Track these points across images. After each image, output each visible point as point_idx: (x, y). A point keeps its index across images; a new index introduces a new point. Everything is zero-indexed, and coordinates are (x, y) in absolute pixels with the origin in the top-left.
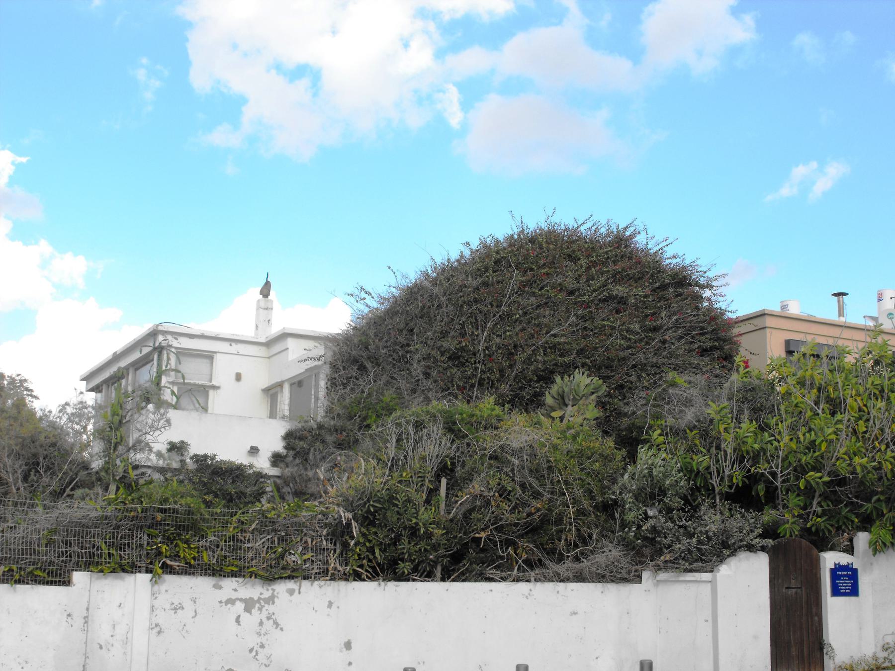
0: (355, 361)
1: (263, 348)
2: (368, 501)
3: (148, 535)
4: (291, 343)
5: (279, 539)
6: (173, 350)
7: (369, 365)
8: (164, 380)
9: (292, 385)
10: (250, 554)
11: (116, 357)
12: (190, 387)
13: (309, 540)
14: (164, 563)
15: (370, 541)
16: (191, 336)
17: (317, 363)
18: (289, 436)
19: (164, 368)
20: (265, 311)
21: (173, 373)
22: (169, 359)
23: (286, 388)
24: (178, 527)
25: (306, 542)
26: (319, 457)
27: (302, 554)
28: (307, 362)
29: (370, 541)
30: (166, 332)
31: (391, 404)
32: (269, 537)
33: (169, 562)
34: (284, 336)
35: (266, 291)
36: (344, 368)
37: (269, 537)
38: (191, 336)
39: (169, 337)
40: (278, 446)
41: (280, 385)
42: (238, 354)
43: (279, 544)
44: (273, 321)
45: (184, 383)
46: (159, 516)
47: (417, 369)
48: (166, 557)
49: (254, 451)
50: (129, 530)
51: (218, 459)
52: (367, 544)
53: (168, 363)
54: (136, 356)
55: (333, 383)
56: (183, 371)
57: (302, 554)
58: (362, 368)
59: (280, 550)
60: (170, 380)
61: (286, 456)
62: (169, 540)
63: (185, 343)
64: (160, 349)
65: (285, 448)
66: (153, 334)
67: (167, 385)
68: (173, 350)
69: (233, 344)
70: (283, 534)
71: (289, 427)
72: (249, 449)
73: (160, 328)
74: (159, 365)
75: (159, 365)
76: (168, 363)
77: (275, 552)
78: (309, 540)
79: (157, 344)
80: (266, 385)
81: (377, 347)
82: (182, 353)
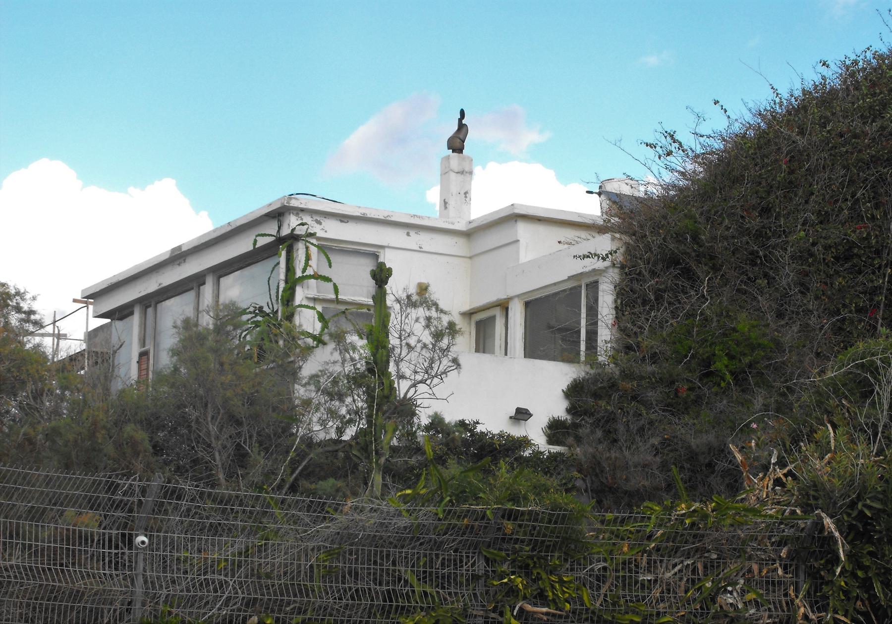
0: (673, 261)
1: (461, 241)
2: (859, 498)
3: (487, 560)
4: (523, 230)
5: (705, 567)
6: (314, 241)
7: (700, 270)
8: (300, 296)
9: (527, 304)
10: (656, 593)
11: (178, 257)
12: (342, 308)
13: (755, 567)
14: (521, 610)
15: (865, 569)
16: (344, 218)
17: (600, 265)
18: (574, 391)
19: (299, 274)
20: (460, 177)
21: (312, 282)
22: (308, 258)
23: (517, 314)
24: (535, 545)
25: (750, 571)
26: (634, 427)
27: (743, 592)
28: (587, 261)
29: (865, 569)
30: (302, 210)
31: (753, 335)
32: (689, 562)
33: (529, 607)
34: (514, 217)
35: (457, 144)
36: (653, 274)
37: (689, 562)
38: (344, 218)
39: (307, 219)
40: (559, 409)
41: (504, 306)
42: (420, 251)
43: (706, 575)
44: (473, 194)
45: (338, 301)
46: (509, 526)
47: (787, 276)
48: (525, 598)
49: (522, 415)
50: (456, 551)
51: (479, 429)
52: (860, 574)
53: (307, 264)
54: (242, 246)
55: (627, 301)
56: (334, 280)
57: (743, 592)
58: (688, 274)
59: (709, 585)
60: (312, 293)
61: (575, 426)
62: (524, 569)
63: (332, 230)
64: (293, 238)
65: (568, 411)
66: (278, 214)
67: (305, 303)
68: (314, 241)
69: (412, 233)
70: (714, 556)
71: (575, 376)
72: (513, 412)
73: (294, 203)
74: (290, 269)
75: (290, 269)
76: (307, 264)
77: (700, 588)
78: (755, 567)
79: (285, 231)
80: (466, 308)
81: (714, 238)
82: (328, 248)
